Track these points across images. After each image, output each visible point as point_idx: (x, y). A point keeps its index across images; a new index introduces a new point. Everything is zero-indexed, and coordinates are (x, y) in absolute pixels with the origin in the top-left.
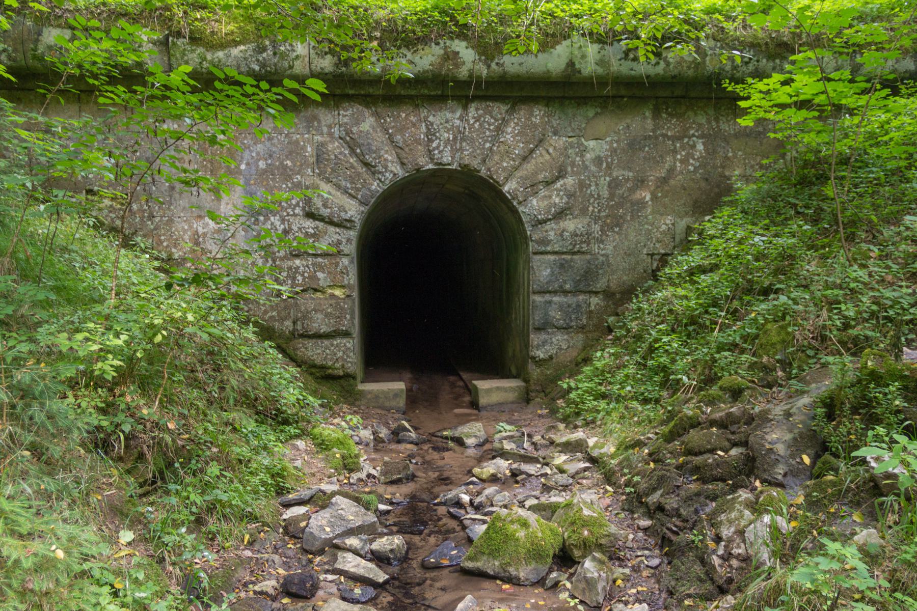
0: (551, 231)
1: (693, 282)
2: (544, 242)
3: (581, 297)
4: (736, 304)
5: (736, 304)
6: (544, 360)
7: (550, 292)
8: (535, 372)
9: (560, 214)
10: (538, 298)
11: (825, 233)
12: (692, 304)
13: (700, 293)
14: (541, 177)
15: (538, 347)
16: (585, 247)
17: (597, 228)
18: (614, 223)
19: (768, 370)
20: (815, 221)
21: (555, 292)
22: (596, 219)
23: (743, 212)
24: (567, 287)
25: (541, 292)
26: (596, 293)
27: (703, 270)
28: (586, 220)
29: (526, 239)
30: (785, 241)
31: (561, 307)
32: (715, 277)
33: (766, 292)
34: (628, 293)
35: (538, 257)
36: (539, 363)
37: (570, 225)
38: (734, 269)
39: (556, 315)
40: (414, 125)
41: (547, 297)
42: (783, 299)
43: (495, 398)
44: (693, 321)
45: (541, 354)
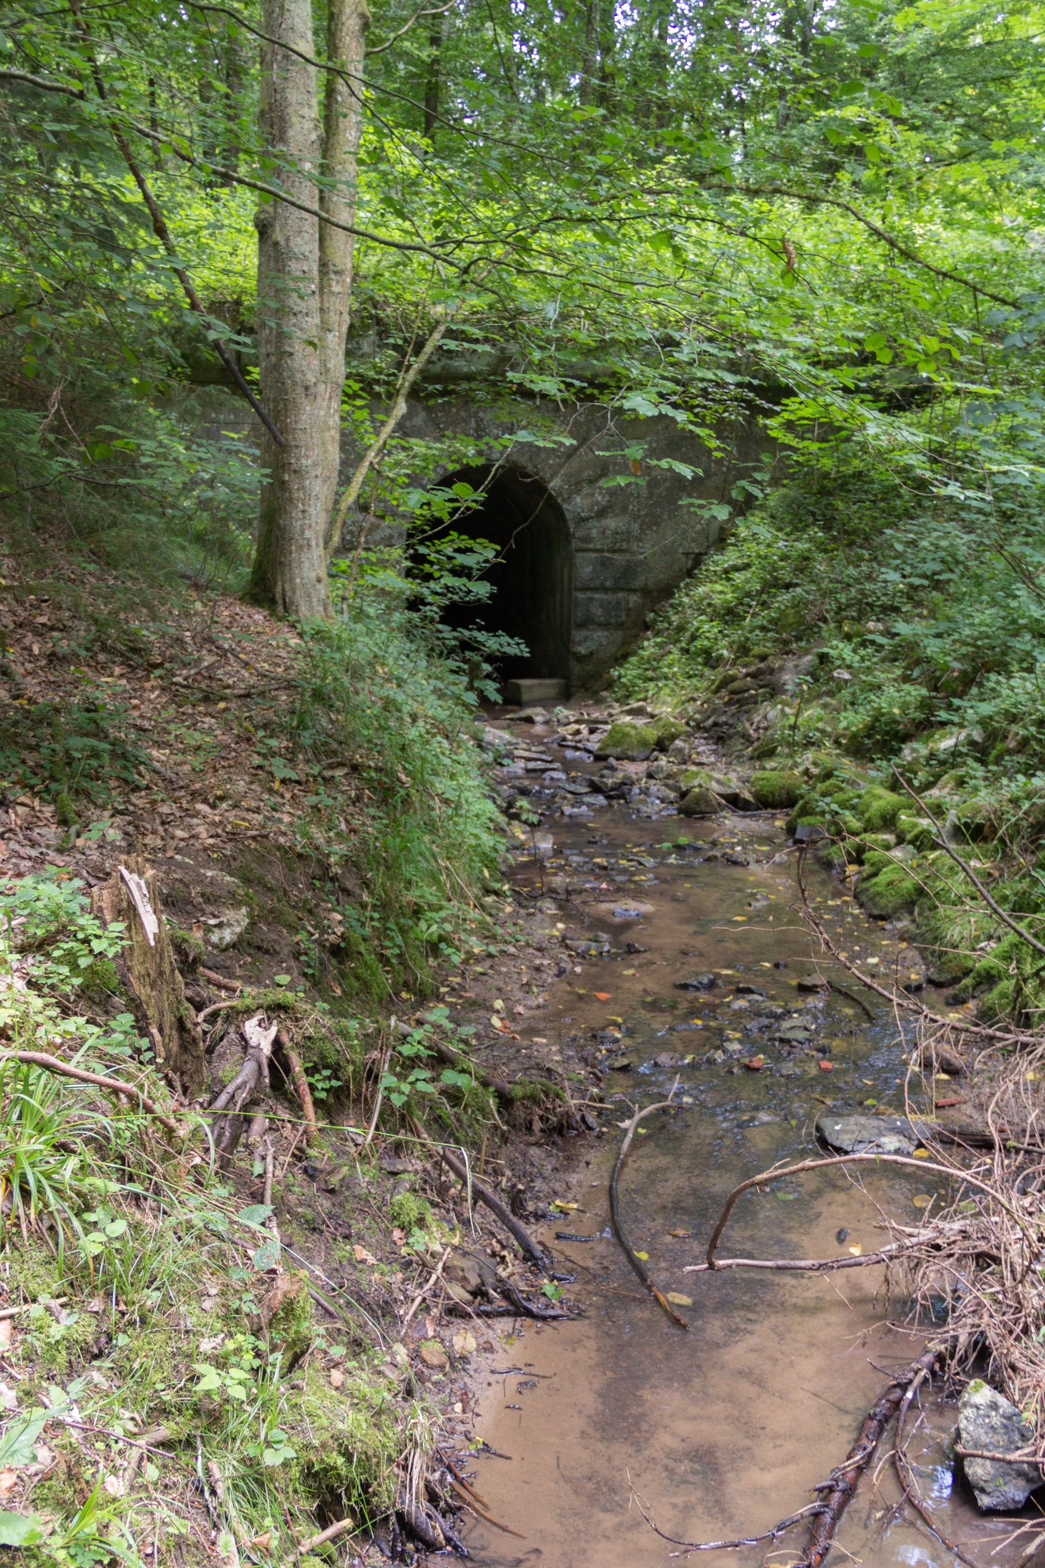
0: (594, 529)
1: (728, 579)
2: (587, 539)
3: (621, 595)
4: (764, 597)
5: (764, 597)
6: (585, 656)
7: (591, 589)
8: (576, 668)
9: (602, 513)
10: (580, 595)
11: (834, 539)
12: (729, 597)
13: (735, 590)
14: (585, 474)
15: (580, 643)
16: (625, 545)
17: (636, 526)
18: (652, 522)
19: (786, 643)
20: (827, 528)
21: (596, 590)
22: (636, 517)
23: (772, 517)
24: (608, 584)
25: (584, 589)
26: (635, 591)
27: (736, 569)
28: (626, 519)
29: (568, 537)
30: (802, 546)
31: (602, 603)
32: (748, 574)
33: (788, 586)
34: (667, 591)
35: (580, 555)
36: (581, 659)
37: (612, 523)
38: (763, 568)
39: (597, 611)
40: (464, 420)
41: (589, 594)
42: (799, 590)
43: (537, 693)
44: (730, 611)
45: (582, 650)
